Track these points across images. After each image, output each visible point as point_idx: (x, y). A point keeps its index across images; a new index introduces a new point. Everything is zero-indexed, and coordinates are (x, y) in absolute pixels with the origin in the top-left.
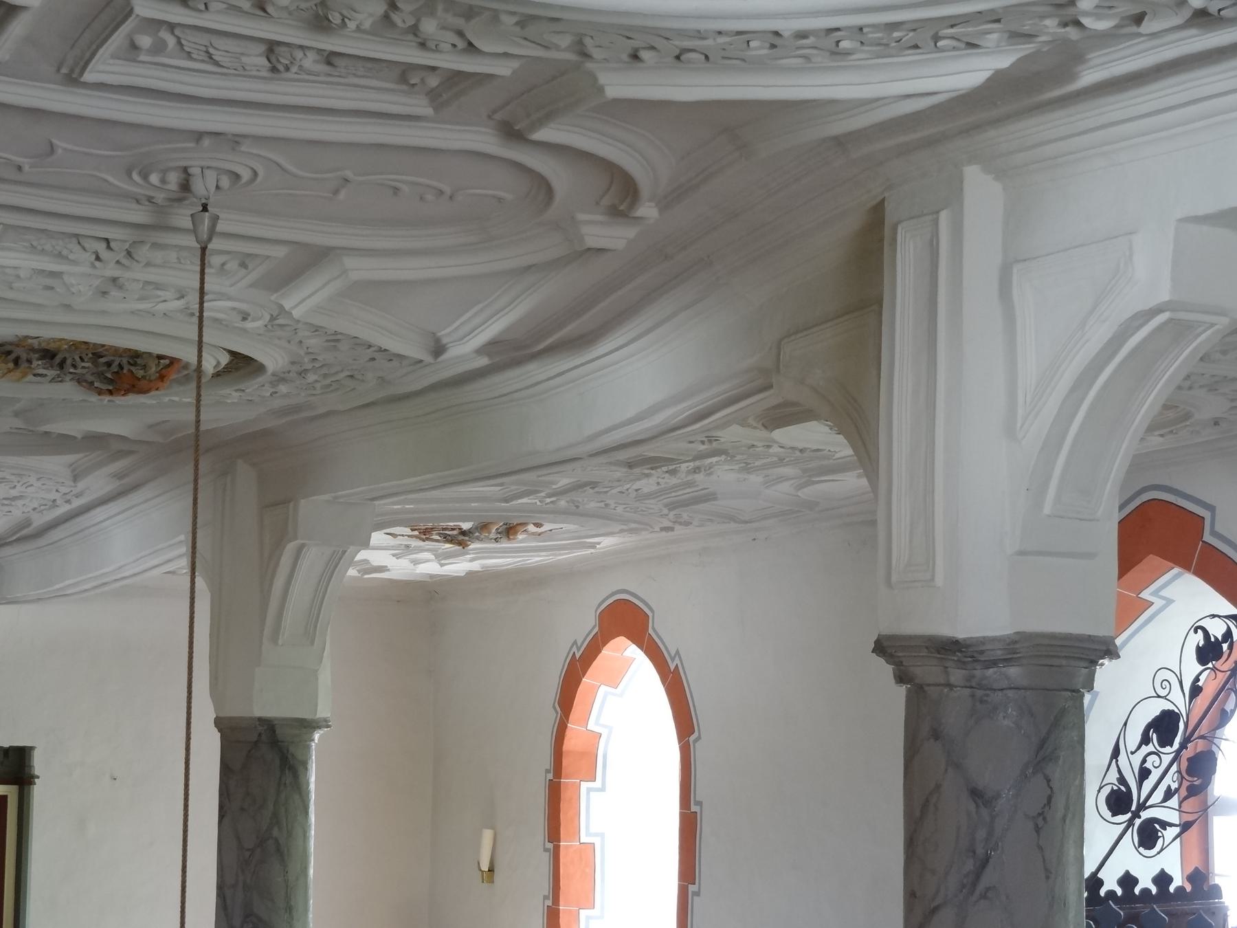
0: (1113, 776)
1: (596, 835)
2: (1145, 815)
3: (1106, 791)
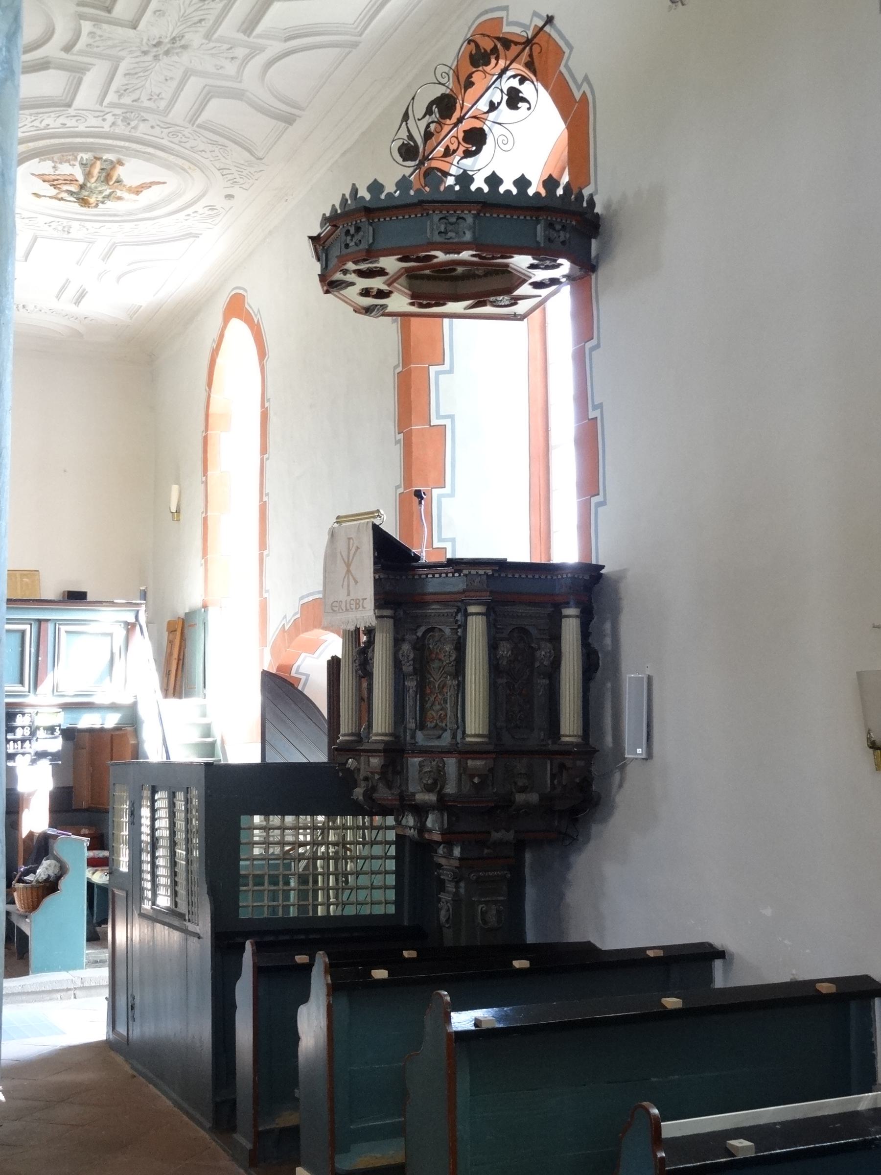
0: (403, 134)
3: (400, 142)
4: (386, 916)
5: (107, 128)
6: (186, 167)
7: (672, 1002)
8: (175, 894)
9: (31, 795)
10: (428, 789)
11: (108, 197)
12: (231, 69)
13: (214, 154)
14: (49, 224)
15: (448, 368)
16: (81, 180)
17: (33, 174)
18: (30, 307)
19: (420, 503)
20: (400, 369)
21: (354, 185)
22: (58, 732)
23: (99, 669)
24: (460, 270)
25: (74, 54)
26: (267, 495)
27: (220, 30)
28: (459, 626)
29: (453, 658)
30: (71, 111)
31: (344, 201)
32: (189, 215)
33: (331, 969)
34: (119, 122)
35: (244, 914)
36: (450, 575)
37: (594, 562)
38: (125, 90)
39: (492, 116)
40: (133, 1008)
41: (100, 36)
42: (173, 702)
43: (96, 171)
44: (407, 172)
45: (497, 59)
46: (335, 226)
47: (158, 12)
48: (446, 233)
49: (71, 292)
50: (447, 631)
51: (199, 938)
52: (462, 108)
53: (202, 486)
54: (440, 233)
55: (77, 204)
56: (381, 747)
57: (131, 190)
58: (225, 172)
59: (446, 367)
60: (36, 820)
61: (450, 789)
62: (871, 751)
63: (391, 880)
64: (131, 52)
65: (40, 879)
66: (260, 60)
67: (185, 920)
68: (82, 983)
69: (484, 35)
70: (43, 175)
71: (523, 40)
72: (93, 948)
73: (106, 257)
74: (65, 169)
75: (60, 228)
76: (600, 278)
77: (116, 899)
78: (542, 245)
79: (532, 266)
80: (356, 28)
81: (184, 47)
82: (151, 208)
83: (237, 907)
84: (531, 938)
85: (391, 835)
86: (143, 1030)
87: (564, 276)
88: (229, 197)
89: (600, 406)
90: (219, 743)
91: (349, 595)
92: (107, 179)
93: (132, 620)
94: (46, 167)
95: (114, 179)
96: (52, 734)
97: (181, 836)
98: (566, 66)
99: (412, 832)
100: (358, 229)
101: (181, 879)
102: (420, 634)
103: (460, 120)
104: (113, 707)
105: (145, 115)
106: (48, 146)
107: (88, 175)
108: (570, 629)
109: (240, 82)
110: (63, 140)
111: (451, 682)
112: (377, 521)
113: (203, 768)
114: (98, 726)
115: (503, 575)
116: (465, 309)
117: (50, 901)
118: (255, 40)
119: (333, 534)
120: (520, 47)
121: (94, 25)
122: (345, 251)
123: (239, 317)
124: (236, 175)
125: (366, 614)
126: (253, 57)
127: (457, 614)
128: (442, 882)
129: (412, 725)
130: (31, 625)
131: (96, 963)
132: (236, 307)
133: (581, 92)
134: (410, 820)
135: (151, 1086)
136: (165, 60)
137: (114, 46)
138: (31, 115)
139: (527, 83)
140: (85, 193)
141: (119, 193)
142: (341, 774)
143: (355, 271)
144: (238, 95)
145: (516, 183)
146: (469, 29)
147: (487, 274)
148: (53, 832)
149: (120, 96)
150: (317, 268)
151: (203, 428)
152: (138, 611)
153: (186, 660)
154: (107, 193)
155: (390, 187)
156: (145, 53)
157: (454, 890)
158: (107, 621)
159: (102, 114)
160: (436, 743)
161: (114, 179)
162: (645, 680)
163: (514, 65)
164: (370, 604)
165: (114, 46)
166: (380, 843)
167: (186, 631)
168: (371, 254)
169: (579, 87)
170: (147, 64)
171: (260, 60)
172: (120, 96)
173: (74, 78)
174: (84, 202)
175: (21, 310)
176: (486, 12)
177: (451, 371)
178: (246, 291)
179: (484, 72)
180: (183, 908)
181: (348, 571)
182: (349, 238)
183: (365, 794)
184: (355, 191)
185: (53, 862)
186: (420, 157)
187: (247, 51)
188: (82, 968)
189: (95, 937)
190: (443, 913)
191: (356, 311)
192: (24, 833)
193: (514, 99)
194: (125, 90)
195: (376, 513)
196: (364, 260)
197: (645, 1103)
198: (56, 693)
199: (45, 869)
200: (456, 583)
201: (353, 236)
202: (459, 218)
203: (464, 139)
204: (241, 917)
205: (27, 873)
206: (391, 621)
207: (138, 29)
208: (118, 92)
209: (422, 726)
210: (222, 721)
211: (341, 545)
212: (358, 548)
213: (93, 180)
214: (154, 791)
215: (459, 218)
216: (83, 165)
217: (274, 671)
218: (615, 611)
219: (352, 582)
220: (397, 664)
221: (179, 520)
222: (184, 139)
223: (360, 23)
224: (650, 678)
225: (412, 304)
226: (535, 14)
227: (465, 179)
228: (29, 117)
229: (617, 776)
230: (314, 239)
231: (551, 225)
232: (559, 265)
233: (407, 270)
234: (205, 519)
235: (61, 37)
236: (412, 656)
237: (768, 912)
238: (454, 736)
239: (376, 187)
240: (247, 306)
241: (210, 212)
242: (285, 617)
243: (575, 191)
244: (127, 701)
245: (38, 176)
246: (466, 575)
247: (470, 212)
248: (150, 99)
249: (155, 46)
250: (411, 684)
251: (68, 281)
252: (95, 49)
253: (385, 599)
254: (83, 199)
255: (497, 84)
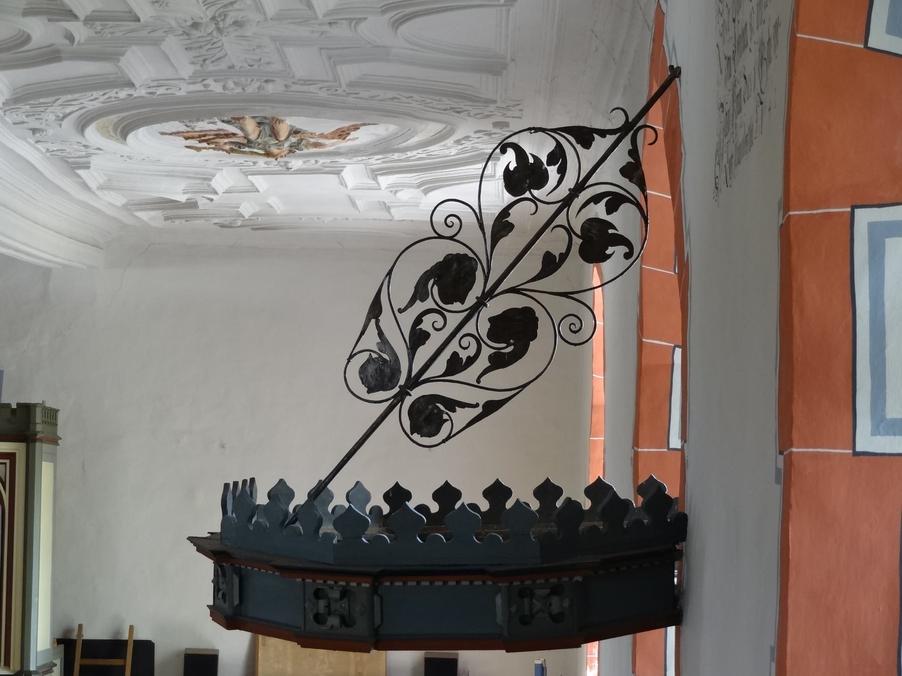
2: (417, 393)
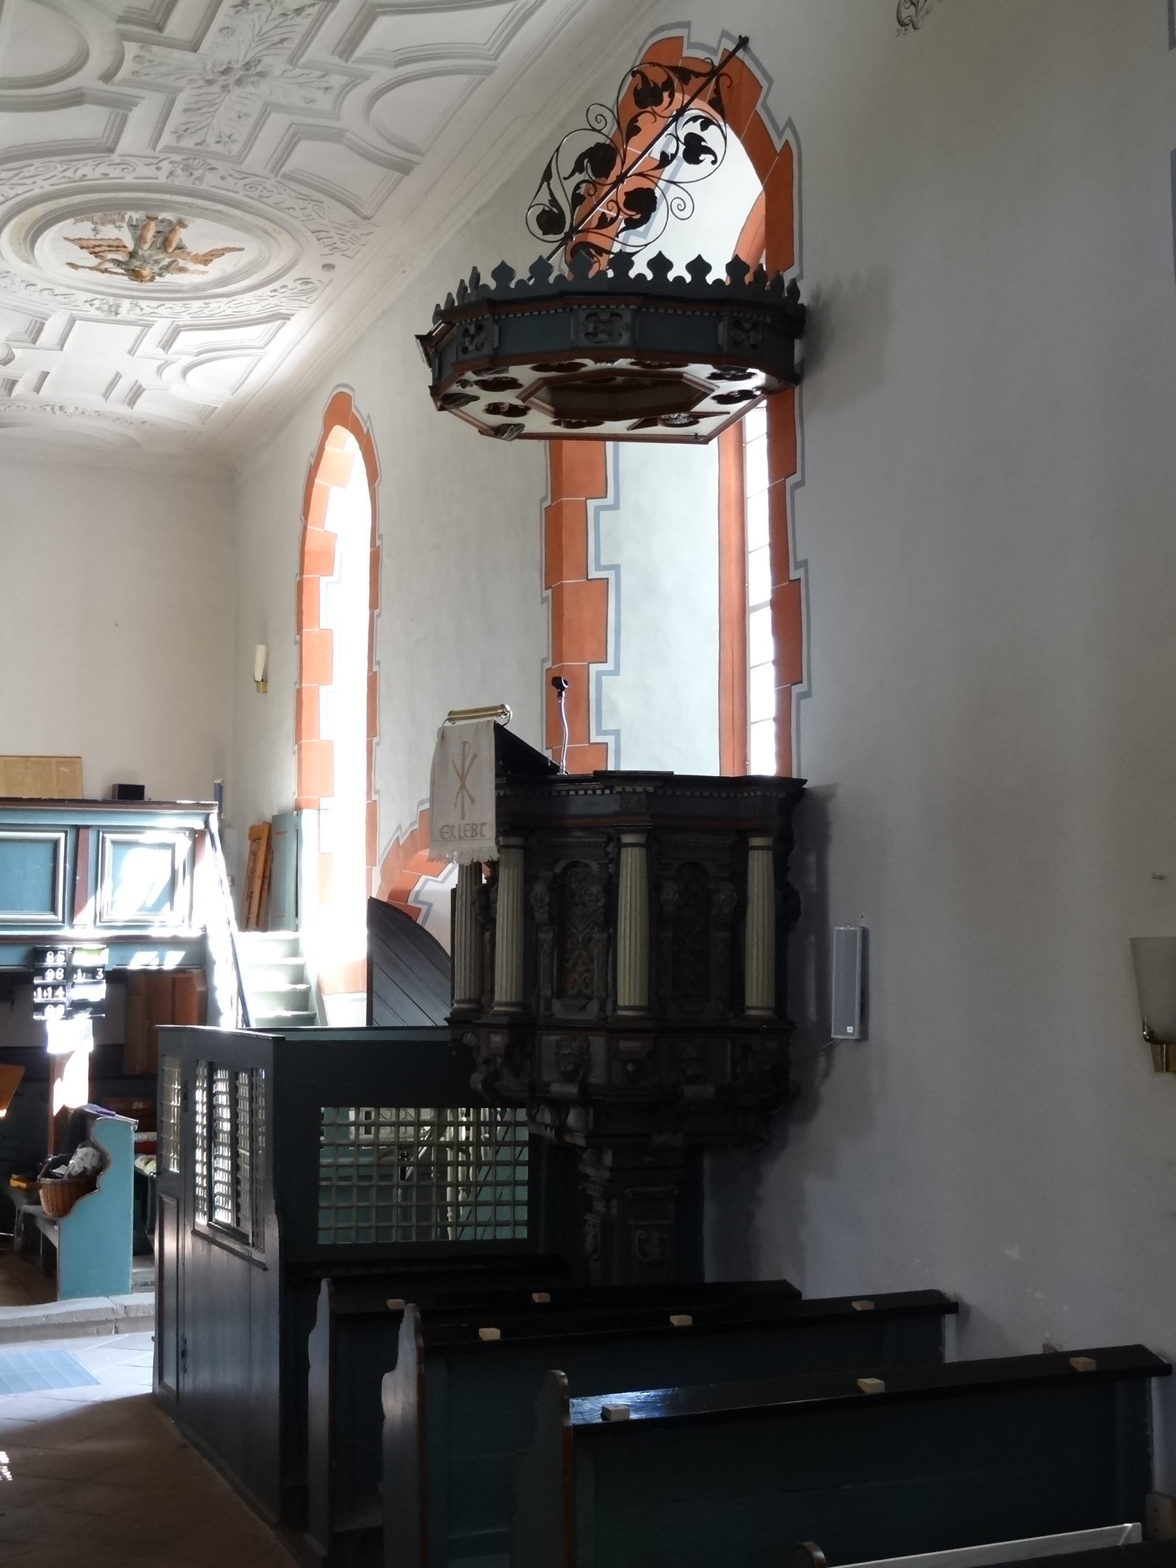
0: (544, 197)
1: (607, 568)
3: (539, 209)
4: (514, 1242)
5: (162, 179)
6: (270, 230)
7: (871, 1384)
8: (237, 1208)
9: (66, 1057)
10: (568, 1078)
11: (166, 268)
12: (324, 102)
13: (306, 212)
14: (90, 302)
15: (612, 503)
16: (131, 246)
17: (66, 239)
18: (71, 409)
19: (560, 695)
20: (548, 503)
21: (475, 268)
22: (100, 975)
23: (156, 888)
24: (620, 379)
25: (113, 85)
26: (378, 663)
27: (309, 50)
28: (611, 861)
29: (600, 904)
30: (115, 157)
31: (462, 288)
32: (275, 291)
33: (422, 1330)
34: (179, 171)
35: (324, 1239)
36: (599, 792)
37: (795, 776)
38: (185, 131)
39: (667, 172)
40: (184, 1354)
41: (151, 61)
42: (255, 936)
43: (150, 235)
44: (545, 249)
45: (672, 96)
46: (450, 325)
47: (226, 30)
48: (595, 334)
49: (123, 387)
50: (595, 867)
51: (265, 1269)
52: (623, 163)
53: (295, 648)
54: (587, 334)
55: (126, 278)
56: (504, 1020)
57: (197, 259)
58: (322, 235)
59: (609, 500)
60: (71, 1091)
61: (597, 1077)
62: (1149, 1044)
63: (522, 1193)
64: (191, 81)
65: (73, 1173)
66: (364, 90)
67: (248, 1244)
68: (127, 1313)
69: (654, 64)
70: (80, 239)
71: (707, 69)
72: (144, 1266)
73: (167, 343)
74: (109, 232)
75: (106, 307)
76: (805, 394)
77: (166, 1207)
78: (725, 350)
79: (714, 376)
80: (489, 50)
81: (262, 75)
82: (224, 281)
83: (314, 1229)
84: (710, 1275)
85: (523, 1134)
86: (200, 1380)
87: (758, 388)
88: (328, 267)
89: (804, 564)
90: (314, 989)
91: (463, 818)
92: (165, 245)
93: (199, 824)
94: (84, 229)
95: (174, 245)
96: (94, 978)
97: (244, 1131)
98: (764, 105)
99: (549, 1133)
100: (480, 328)
101: (245, 1187)
102: (558, 870)
103: (621, 178)
104: (175, 943)
105: (213, 163)
106: (85, 203)
107: (139, 240)
108: (759, 867)
109: (338, 119)
110: (105, 195)
111: (599, 936)
112: (501, 720)
113: (271, 1047)
114: (154, 967)
115: (669, 792)
116: (628, 429)
117: (87, 1205)
118: (355, 66)
119: (443, 736)
120: (703, 80)
121: (142, 47)
122: (462, 357)
123: (345, 425)
124: (336, 238)
125: (486, 846)
126: (354, 86)
127: (607, 844)
128: (590, 1199)
129: (546, 991)
130: (66, 833)
131: (142, 1286)
132: (341, 411)
133: (783, 140)
134: (547, 1117)
135: (205, 1461)
136: (237, 91)
137: (168, 74)
138: (61, 162)
139: (712, 128)
140: (136, 263)
141: (181, 263)
142: (454, 1054)
143: (477, 383)
144: (335, 136)
145: (690, 267)
146: (640, 51)
147: (655, 385)
148: (93, 1109)
149: (179, 138)
150: (426, 376)
151: (297, 570)
152: (208, 815)
153: (273, 880)
154: (167, 261)
155: (522, 273)
156: (210, 82)
157: (603, 1210)
158: (168, 828)
159: (156, 161)
160: (577, 1016)
161: (174, 245)
162: (859, 935)
163: (697, 102)
164: (490, 831)
165: (168, 74)
166: (508, 1144)
167: (273, 841)
168: (498, 361)
169: (780, 134)
170: (214, 96)
171: (364, 90)
172: (179, 138)
173: (117, 115)
174: (135, 275)
175: (58, 412)
176: (662, 29)
177: (615, 506)
178: (352, 389)
179: (654, 113)
180: (247, 1228)
181: (463, 787)
182: (467, 340)
183: (485, 1083)
184: (476, 276)
185: (90, 1150)
186: (567, 229)
187: (345, 79)
188: (126, 1292)
189: (143, 1250)
190: (589, 1239)
191: (481, 432)
192: (56, 1109)
193: (695, 150)
194: (185, 131)
195: (500, 709)
196: (488, 370)
197: (806, 1544)
198: (98, 924)
199: (81, 1159)
200: (606, 803)
201: (473, 337)
202: (613, 315)
203: (626, 205)
204: (321, 1242)
205: (56, 1164)
206: (521, 852)
207: (200, 51)
208: (176, 132)
209: (560, 993)
210: (308, 968)
211: (454, 750)
212: (475, 756)
213: (146, 246)
214: (212, 1070)
215: (613, 315)
216: (133, 227)
217: (385, 899)
218: (821, 838)
219: (467, 801)
220: (527, 909)
221: (265, 692)
222: (265, 194)
223: (496, 41)
224: (865, 933)
225: (557, 423)
226: (725, 34)
227: (624, 261)
228: (59, 166)
229: (822, 1061)
230: (424, 340)
231: (737, 324)
232: (750, 376)
233: (546, 382)
234: (299, 692)
235: (98, 61)
236: (547, 899)
237: (1014, 1253)
238: (602, 1008)
239: (503, 272)
240: (353, 410)
241: (305, 287)
242: (399, 827)
243: (771, 277)
244: (196, 933)
245: (73, 241)
246: (618, 793)
247: (627, 306)
248: (218, 142)
249: (223, 73)
250: (546, 937)
251: (118, 376)
252: (144, 78)
253: (509, 822)
254: (134, 271)
255: (671, 130)
